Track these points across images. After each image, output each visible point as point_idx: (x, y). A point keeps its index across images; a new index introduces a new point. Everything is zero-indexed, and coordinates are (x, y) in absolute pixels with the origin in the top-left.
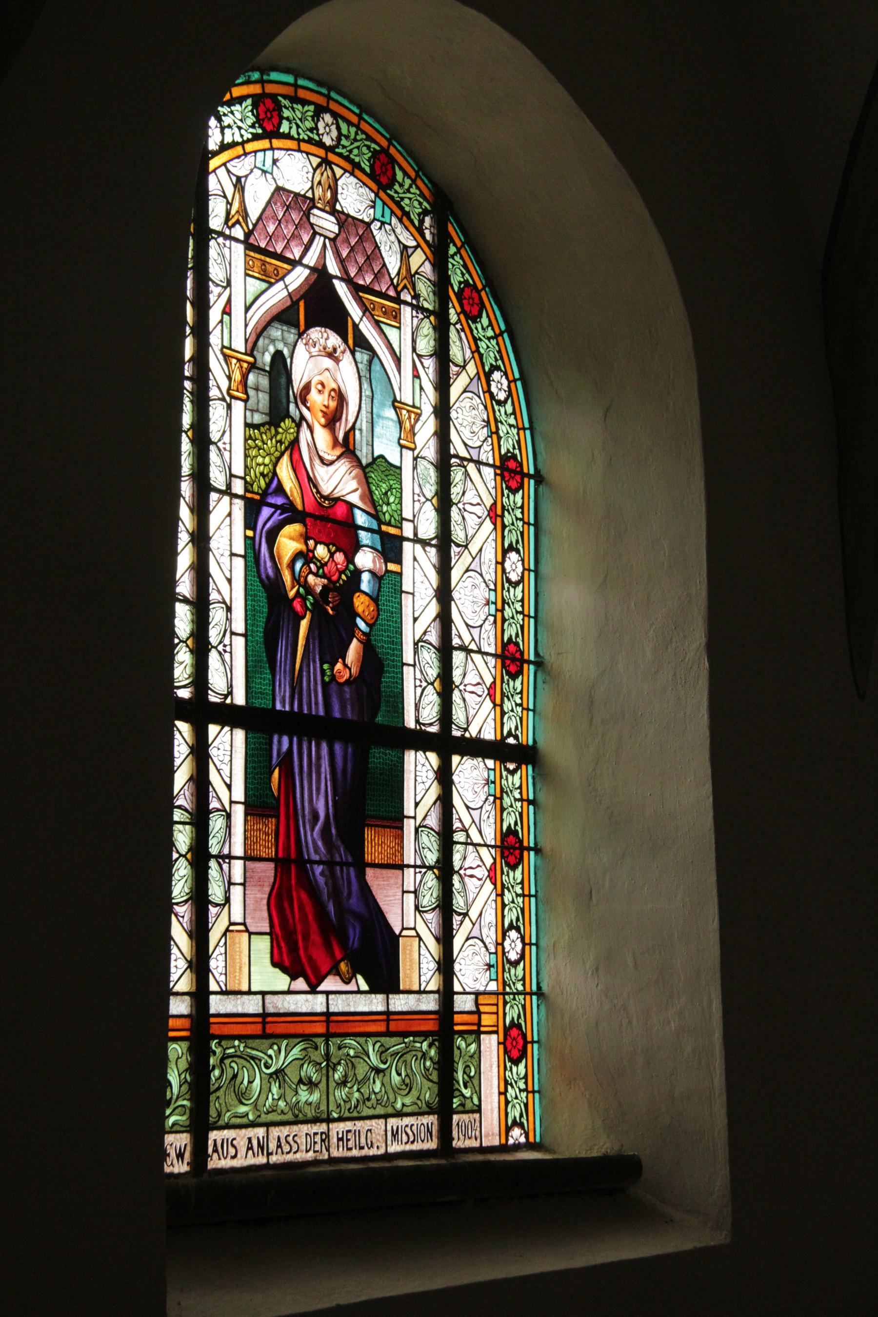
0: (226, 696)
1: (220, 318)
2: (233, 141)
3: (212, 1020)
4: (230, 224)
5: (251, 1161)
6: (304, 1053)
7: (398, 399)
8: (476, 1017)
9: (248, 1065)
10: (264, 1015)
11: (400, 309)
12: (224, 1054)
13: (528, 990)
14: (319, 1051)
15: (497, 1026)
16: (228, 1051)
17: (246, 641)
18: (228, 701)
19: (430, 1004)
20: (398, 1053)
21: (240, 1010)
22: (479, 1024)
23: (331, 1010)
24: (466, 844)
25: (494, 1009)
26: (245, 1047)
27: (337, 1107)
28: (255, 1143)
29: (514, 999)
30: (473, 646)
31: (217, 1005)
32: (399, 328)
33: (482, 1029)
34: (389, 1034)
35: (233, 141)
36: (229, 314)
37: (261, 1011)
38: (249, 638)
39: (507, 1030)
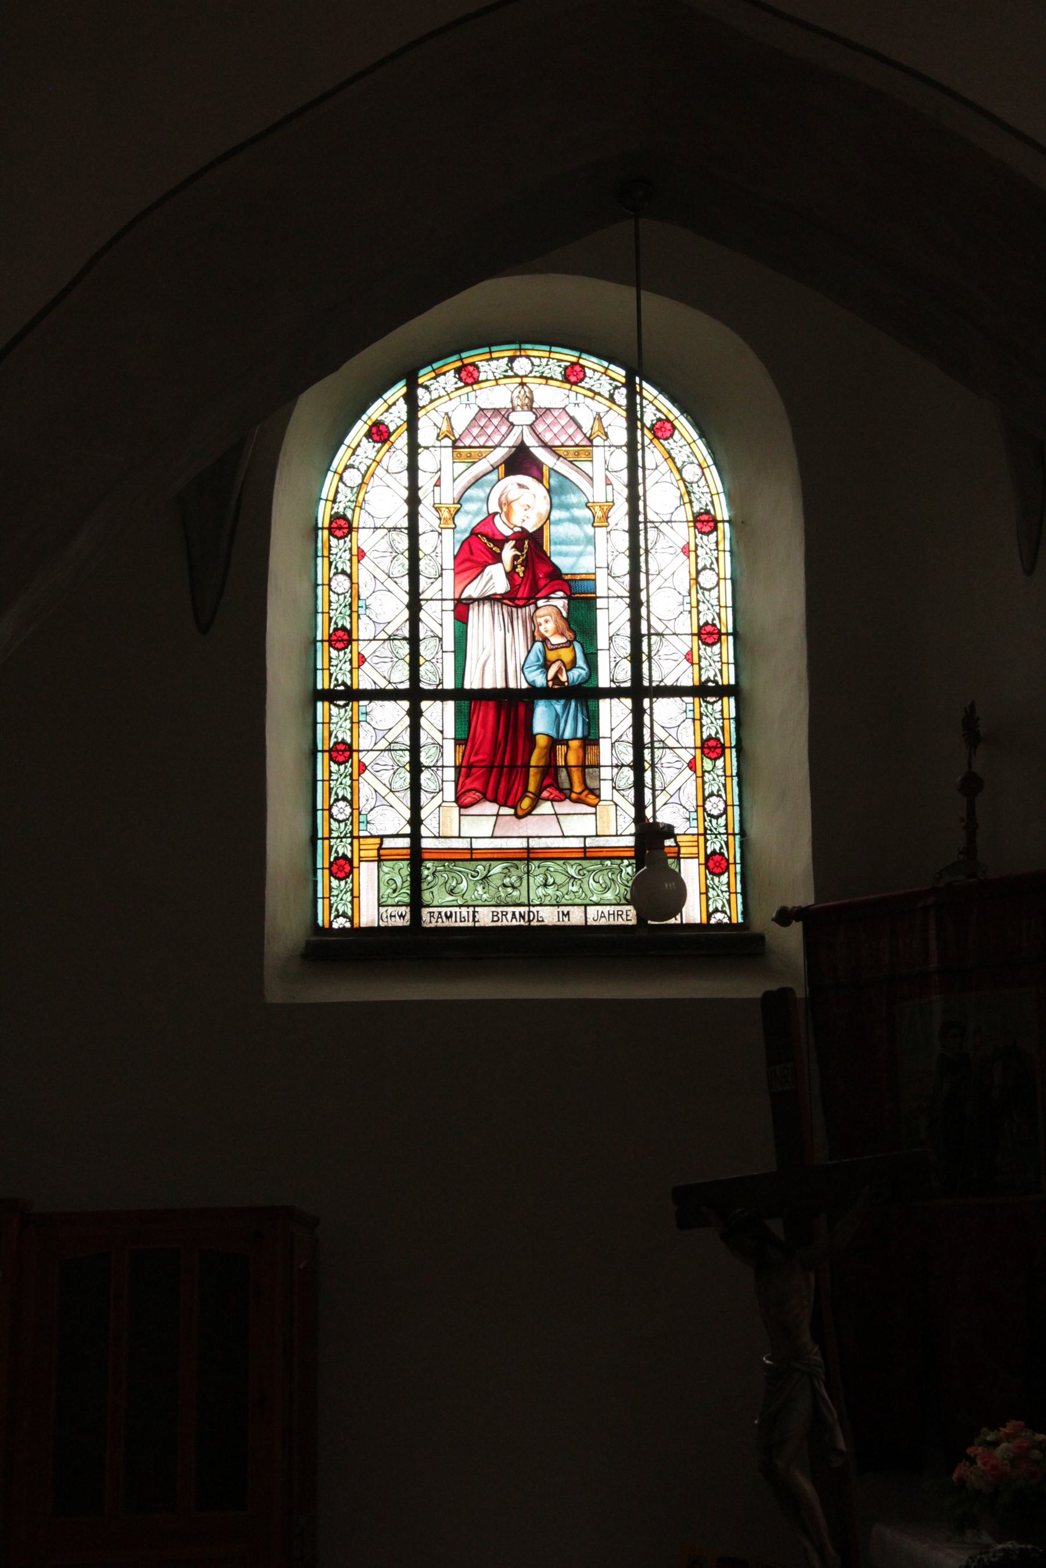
0: (438, 685)
1: (432, 489)
2: (672, 438)
3: (423, 851)
4: (440, 438)
5: (514, 923)
6: (506, 871)
7: (591, 501)
8: (677, 849)
9: (457, 876)
10: (585, 848)
11: (592, 450)
12: (436, 870)
13: (730, 831)
14: (520, 870)
15: (698, 854)
16: (438, 868)
17: (455, 654)
18: (440, 687)
19: (406, 842)
20: (595, 871)
21: (601, 845)
22: (679, 852)
23: (530, 847)
24: (663, 748)
25: (696, 844)
26: (612, 864)
27: (538, 899)
28: (443, 914)
29: (716, 837)
30: (667, 632)
31: (425, 843)
32: (592, 461)
33: (681, 856)
34: (585, 858)
35: (672, 438)
36: (439, 486)
37: (469, 847)
38: (457, 653)
39: (707, 857)
